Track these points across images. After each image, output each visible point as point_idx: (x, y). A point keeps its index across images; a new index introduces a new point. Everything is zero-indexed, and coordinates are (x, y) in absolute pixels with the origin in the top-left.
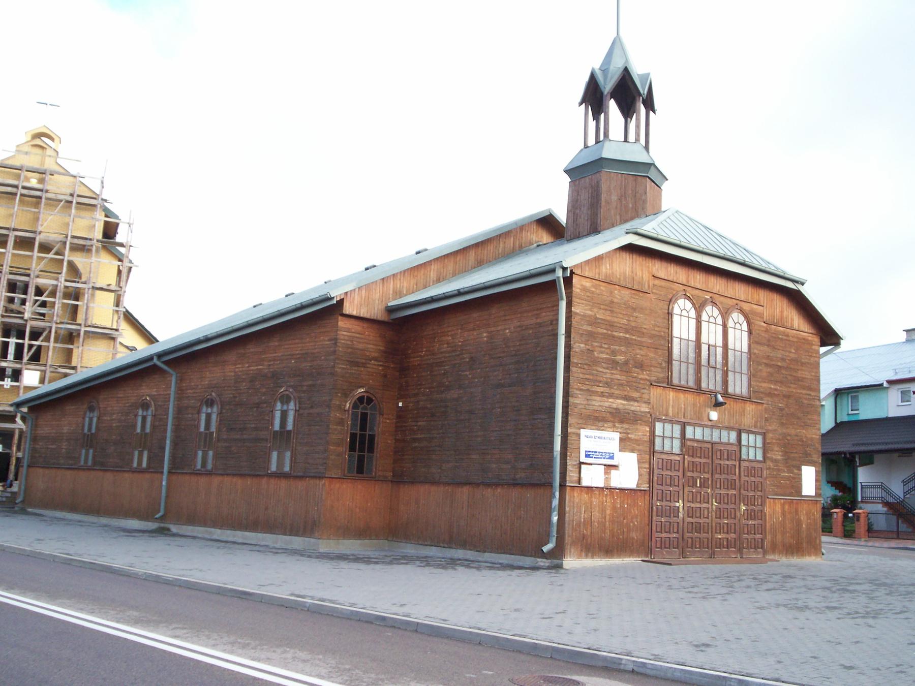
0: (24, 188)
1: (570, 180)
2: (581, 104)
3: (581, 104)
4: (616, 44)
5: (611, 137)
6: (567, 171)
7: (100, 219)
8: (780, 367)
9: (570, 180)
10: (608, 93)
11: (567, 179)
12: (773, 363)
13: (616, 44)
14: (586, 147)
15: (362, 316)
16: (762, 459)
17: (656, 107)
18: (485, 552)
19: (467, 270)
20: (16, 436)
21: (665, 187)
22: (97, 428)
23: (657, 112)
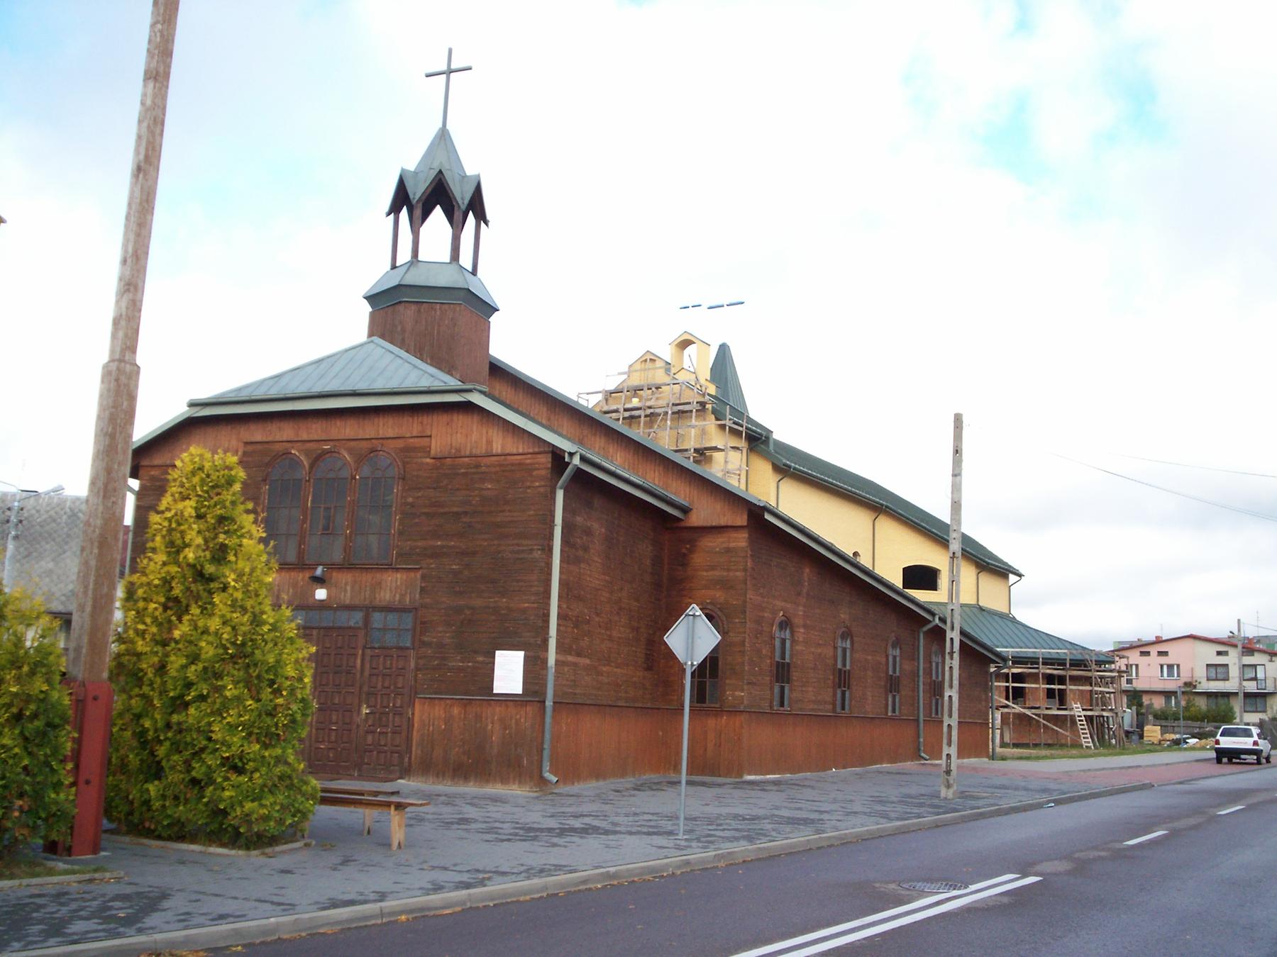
0: (626, 410)
1: (371, 310)
2: (388, 214)
3: (388, 214)
4: (443, 137)
5: (420, 259)
6: (372, 299)
7: (111, 364)
8: (457, 513)
9: (371, 310)
10: (418, 202)
11: (367, 308)
12: (446, 510)
13: (443, 137)
14: (394, 267)
15: (714, 524)
16: (411, 615)
17: (489, 217)
18: (826, 768)
19: (738, 472)
20: (1011, 697)
21: (494, 319)
22: (792, 656)
23: (490, 224)
